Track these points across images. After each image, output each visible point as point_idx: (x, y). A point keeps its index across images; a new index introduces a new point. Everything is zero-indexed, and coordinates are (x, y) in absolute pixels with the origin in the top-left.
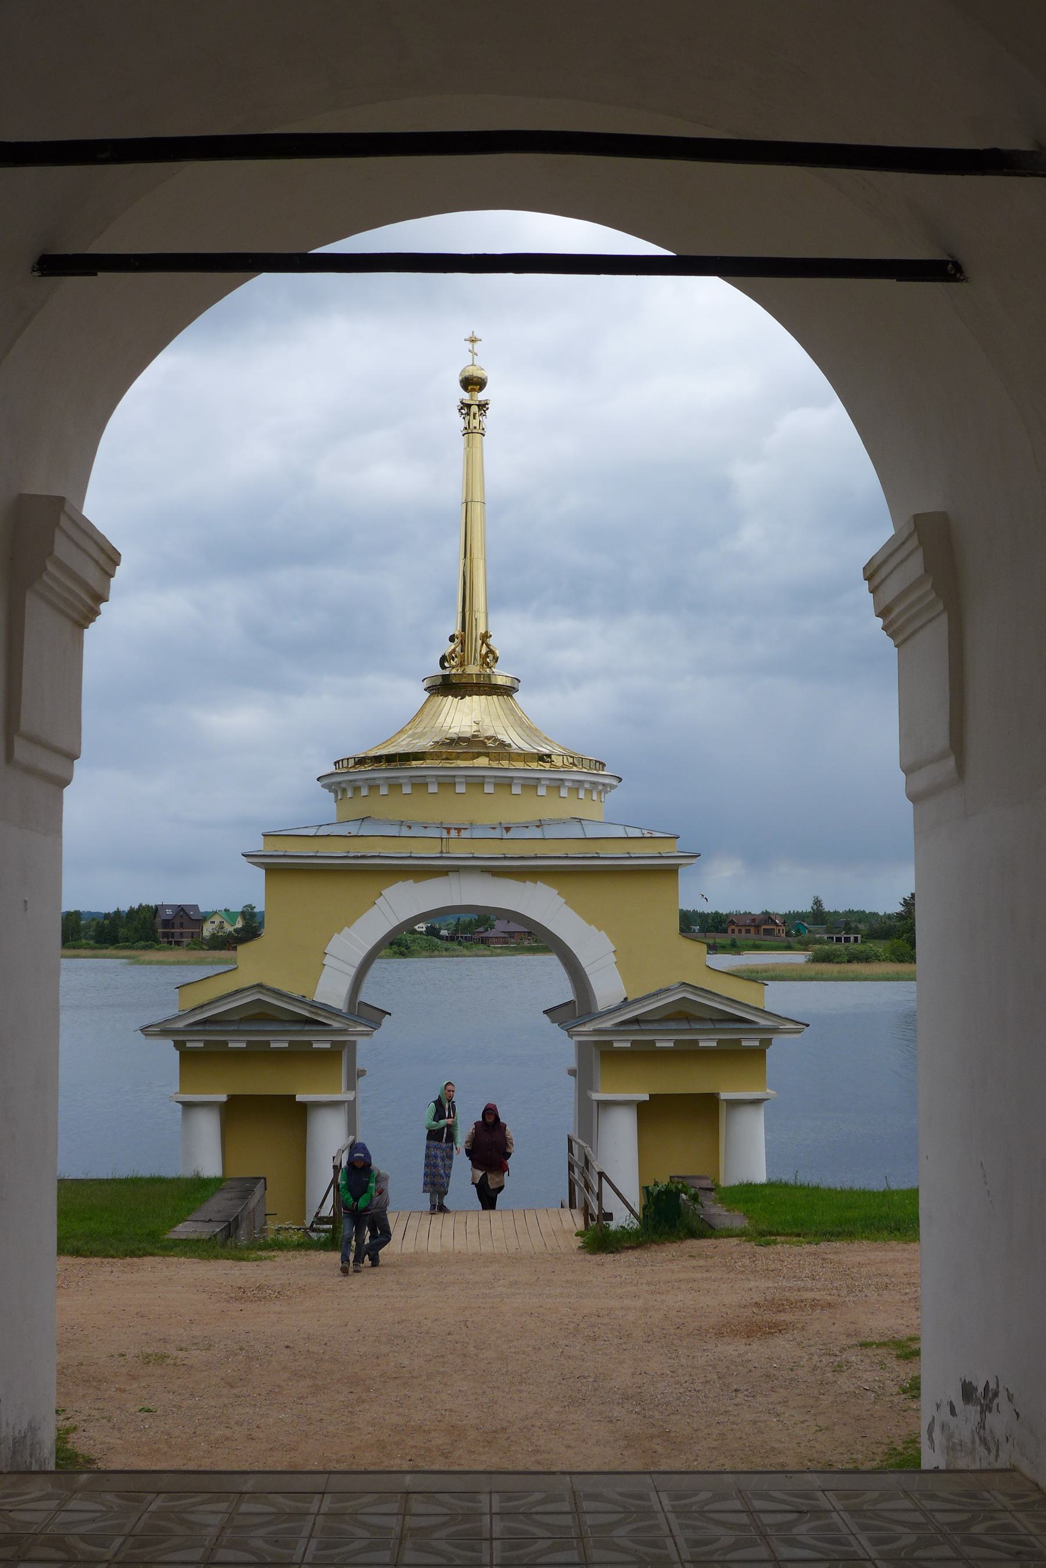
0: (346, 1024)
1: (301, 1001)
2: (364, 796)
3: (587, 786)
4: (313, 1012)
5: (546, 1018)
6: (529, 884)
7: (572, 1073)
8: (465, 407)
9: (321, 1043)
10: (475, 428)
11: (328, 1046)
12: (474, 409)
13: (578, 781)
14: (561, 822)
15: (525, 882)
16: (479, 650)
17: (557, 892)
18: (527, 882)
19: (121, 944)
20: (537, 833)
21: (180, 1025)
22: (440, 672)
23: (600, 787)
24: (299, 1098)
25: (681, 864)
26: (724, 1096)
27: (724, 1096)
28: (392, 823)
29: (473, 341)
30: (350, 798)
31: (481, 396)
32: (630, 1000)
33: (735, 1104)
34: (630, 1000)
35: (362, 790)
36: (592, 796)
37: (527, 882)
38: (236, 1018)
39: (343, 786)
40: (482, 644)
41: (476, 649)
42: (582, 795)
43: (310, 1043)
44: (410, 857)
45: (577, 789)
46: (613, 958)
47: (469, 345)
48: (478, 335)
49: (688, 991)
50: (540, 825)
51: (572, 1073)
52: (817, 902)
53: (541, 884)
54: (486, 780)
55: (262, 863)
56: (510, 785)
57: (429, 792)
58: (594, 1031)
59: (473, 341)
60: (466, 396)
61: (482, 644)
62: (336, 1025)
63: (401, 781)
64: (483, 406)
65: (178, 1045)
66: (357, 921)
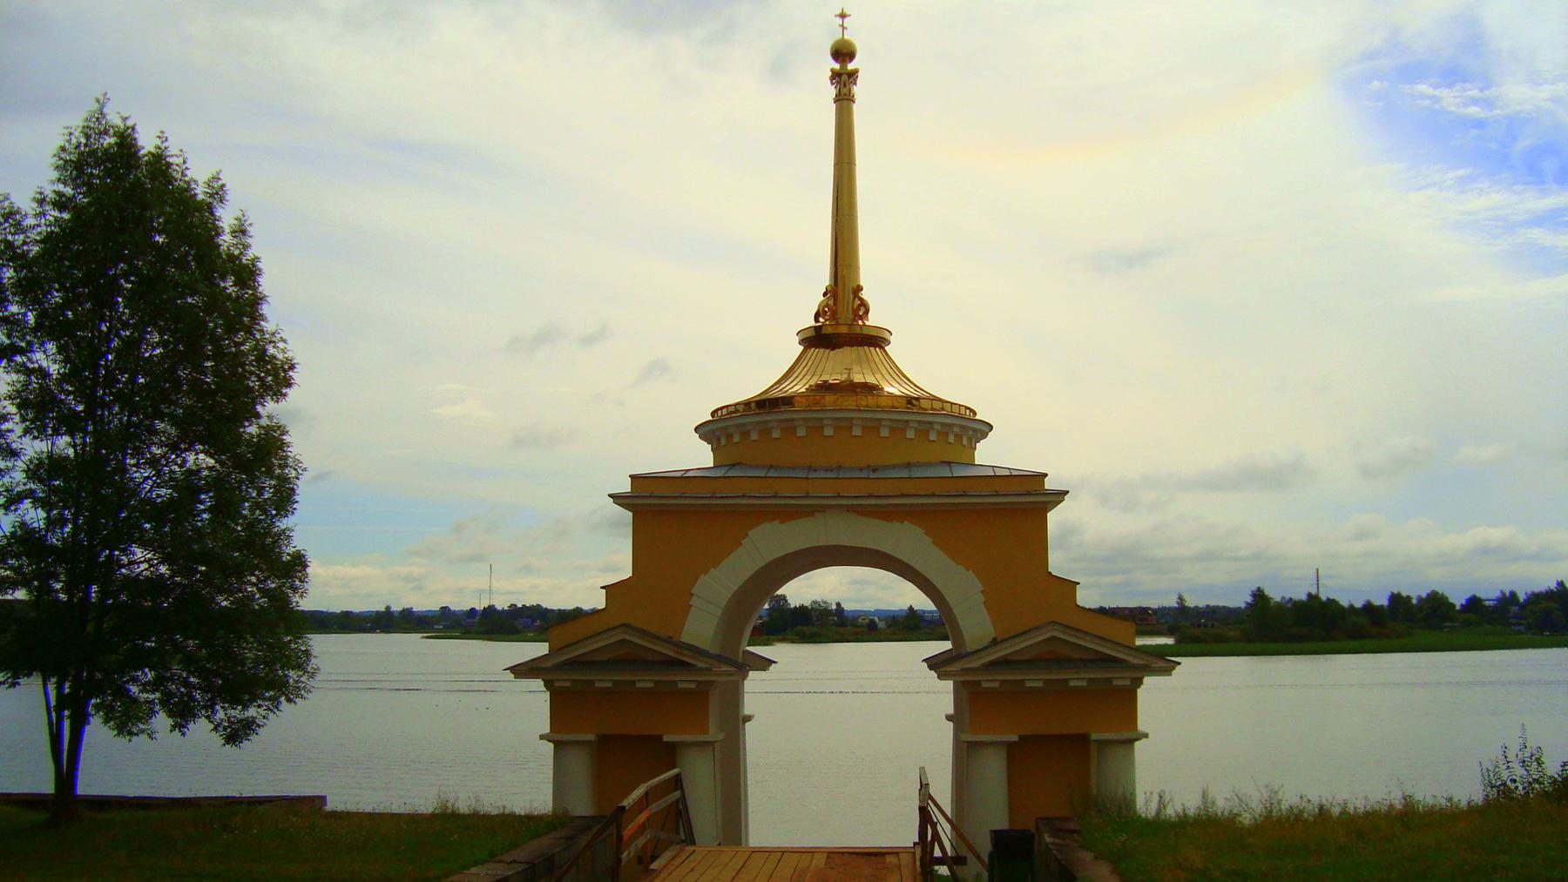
0: (706, 663)
1: (668, 641)
2: (800, 437)
3: (956, 430)
4: (678, 653)
5: (925, 664)
6: (896, 524)
7: (949, 718)
8: (836, 76)
9: (686, 682)
10: (845, 95)
11: (693, 686)
12: (844, 78)
13: (947, 425)
14: (893, 467)
15: (902, 522)
16: (851, 304)
17: (931, 540)
18: (906, 523)
19: (790, 637)
20: (905, 474)
21: (549, 664)
22: (813, 323)
23: (971, 433)
24: (665, 738)
25: (1049, 502)
26: (1094, 736)
27: (1094, 736)
28: (762, 467)
29: (843, 16)
30: (736, 443)
31: (851, 67)
32: (998, 640)
33: (1103, 744)
34: (998, 640)
35: (752, 434)
36: (962, 441)
37: (906, 523)
38: (605, 658)
39: (718, 433)
40: (854, 299)
41: (848, 303)
42: (951, 439)
43: (675, 682)
44: (651, 497)
45: (947, 434)
46: (981, 599)
47: (839, 21)
48: (847, 11)
49: (1056, 630)
50: (908, 466)
51: (949, 718)
52: (1181, 598)
53: (909, 525)
54: (883, 424)
55: (629, 504)
56: (878, 428)
57: (853, 434)
58: (963, 670)
59: (843, 16)
60: (837, 66)
61: (854, 299)
62: (700, 665)
63: (770, 425)
64: (853, 75)
65: (548, 684)
66: (911, 584)
